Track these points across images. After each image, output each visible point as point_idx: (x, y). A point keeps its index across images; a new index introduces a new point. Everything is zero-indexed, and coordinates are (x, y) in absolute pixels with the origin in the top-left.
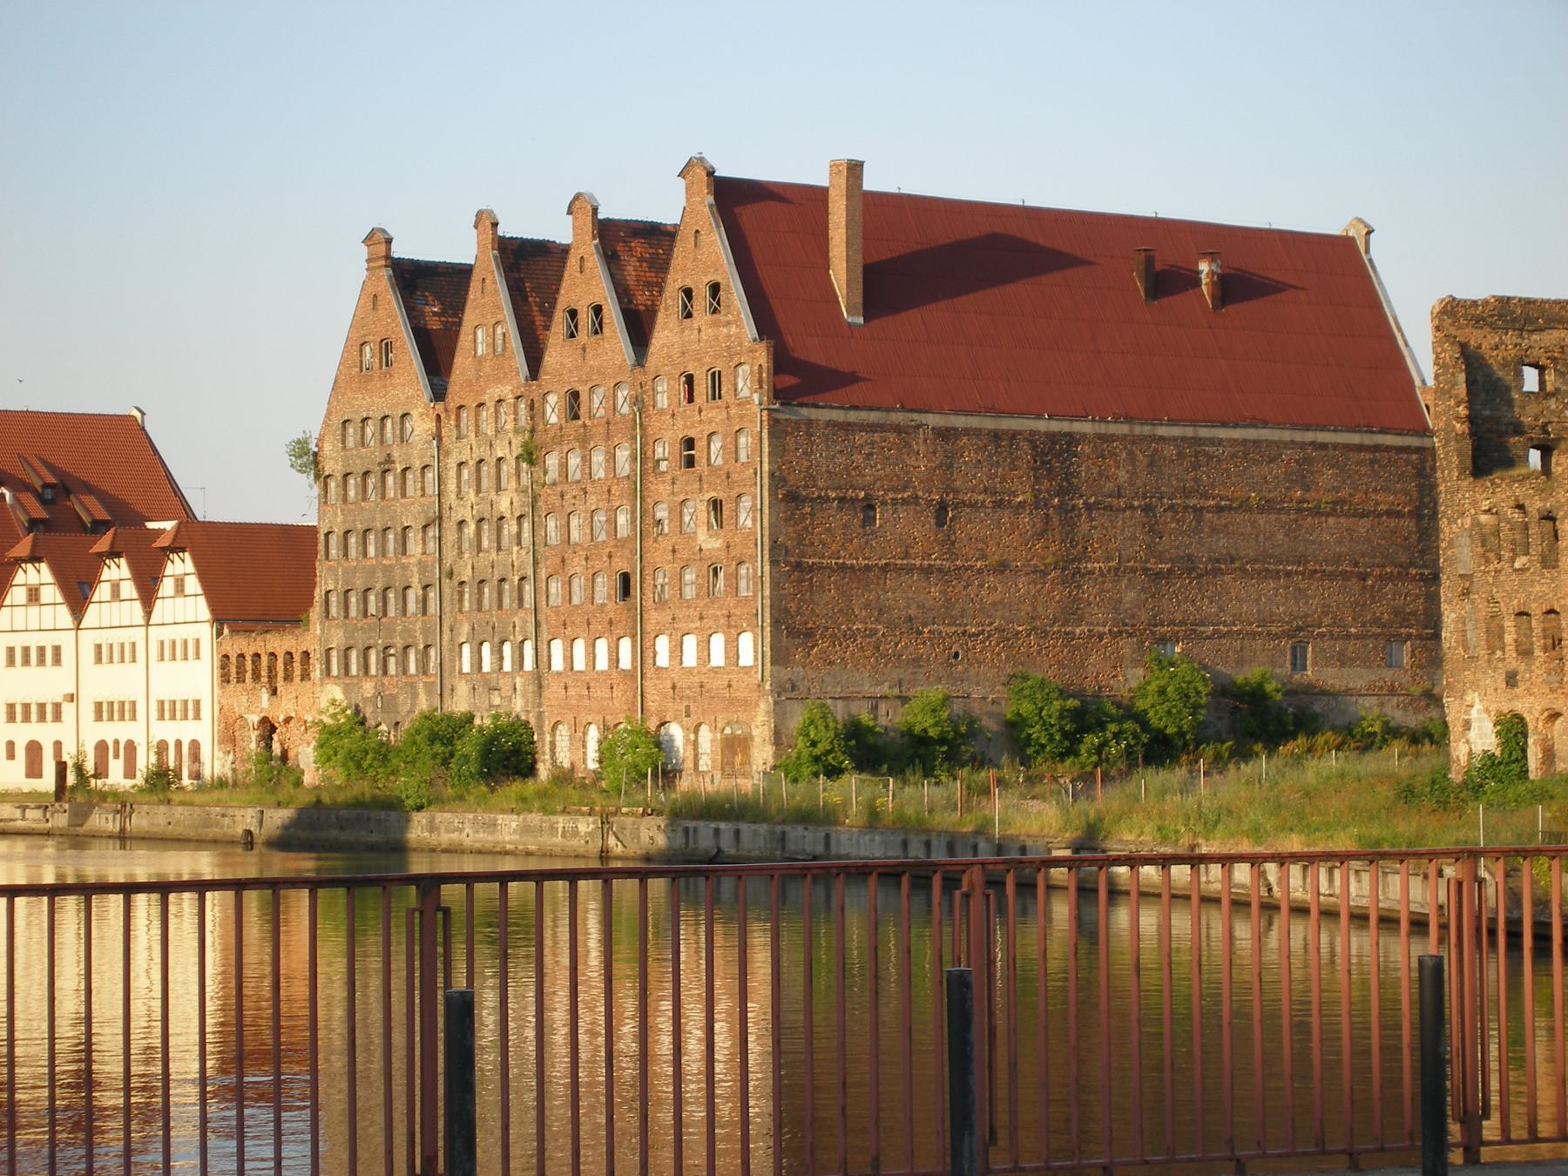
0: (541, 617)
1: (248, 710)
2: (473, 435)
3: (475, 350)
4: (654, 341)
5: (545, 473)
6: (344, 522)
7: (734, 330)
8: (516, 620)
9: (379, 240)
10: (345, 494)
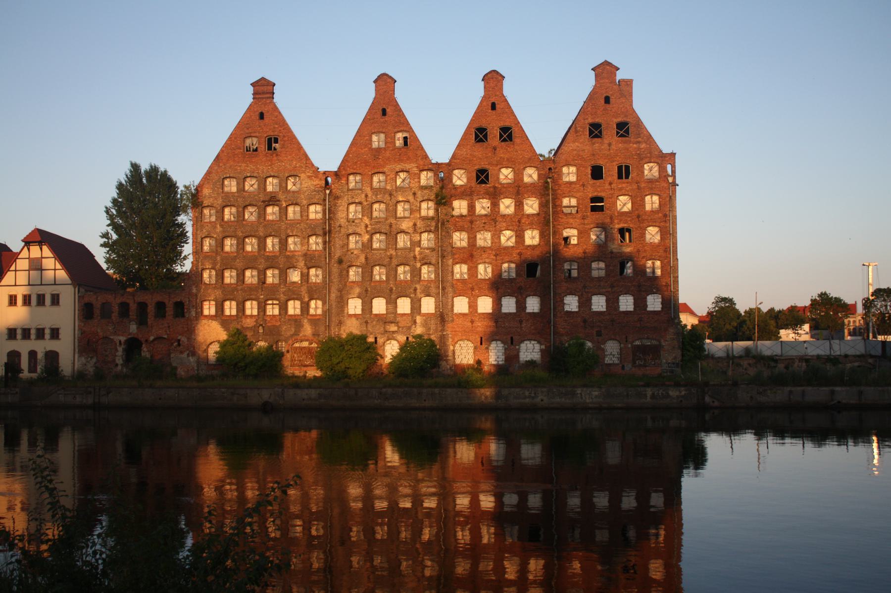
1: (115, 334)
6: (224, 232)
7: (643, 146)
8: (418, 286)
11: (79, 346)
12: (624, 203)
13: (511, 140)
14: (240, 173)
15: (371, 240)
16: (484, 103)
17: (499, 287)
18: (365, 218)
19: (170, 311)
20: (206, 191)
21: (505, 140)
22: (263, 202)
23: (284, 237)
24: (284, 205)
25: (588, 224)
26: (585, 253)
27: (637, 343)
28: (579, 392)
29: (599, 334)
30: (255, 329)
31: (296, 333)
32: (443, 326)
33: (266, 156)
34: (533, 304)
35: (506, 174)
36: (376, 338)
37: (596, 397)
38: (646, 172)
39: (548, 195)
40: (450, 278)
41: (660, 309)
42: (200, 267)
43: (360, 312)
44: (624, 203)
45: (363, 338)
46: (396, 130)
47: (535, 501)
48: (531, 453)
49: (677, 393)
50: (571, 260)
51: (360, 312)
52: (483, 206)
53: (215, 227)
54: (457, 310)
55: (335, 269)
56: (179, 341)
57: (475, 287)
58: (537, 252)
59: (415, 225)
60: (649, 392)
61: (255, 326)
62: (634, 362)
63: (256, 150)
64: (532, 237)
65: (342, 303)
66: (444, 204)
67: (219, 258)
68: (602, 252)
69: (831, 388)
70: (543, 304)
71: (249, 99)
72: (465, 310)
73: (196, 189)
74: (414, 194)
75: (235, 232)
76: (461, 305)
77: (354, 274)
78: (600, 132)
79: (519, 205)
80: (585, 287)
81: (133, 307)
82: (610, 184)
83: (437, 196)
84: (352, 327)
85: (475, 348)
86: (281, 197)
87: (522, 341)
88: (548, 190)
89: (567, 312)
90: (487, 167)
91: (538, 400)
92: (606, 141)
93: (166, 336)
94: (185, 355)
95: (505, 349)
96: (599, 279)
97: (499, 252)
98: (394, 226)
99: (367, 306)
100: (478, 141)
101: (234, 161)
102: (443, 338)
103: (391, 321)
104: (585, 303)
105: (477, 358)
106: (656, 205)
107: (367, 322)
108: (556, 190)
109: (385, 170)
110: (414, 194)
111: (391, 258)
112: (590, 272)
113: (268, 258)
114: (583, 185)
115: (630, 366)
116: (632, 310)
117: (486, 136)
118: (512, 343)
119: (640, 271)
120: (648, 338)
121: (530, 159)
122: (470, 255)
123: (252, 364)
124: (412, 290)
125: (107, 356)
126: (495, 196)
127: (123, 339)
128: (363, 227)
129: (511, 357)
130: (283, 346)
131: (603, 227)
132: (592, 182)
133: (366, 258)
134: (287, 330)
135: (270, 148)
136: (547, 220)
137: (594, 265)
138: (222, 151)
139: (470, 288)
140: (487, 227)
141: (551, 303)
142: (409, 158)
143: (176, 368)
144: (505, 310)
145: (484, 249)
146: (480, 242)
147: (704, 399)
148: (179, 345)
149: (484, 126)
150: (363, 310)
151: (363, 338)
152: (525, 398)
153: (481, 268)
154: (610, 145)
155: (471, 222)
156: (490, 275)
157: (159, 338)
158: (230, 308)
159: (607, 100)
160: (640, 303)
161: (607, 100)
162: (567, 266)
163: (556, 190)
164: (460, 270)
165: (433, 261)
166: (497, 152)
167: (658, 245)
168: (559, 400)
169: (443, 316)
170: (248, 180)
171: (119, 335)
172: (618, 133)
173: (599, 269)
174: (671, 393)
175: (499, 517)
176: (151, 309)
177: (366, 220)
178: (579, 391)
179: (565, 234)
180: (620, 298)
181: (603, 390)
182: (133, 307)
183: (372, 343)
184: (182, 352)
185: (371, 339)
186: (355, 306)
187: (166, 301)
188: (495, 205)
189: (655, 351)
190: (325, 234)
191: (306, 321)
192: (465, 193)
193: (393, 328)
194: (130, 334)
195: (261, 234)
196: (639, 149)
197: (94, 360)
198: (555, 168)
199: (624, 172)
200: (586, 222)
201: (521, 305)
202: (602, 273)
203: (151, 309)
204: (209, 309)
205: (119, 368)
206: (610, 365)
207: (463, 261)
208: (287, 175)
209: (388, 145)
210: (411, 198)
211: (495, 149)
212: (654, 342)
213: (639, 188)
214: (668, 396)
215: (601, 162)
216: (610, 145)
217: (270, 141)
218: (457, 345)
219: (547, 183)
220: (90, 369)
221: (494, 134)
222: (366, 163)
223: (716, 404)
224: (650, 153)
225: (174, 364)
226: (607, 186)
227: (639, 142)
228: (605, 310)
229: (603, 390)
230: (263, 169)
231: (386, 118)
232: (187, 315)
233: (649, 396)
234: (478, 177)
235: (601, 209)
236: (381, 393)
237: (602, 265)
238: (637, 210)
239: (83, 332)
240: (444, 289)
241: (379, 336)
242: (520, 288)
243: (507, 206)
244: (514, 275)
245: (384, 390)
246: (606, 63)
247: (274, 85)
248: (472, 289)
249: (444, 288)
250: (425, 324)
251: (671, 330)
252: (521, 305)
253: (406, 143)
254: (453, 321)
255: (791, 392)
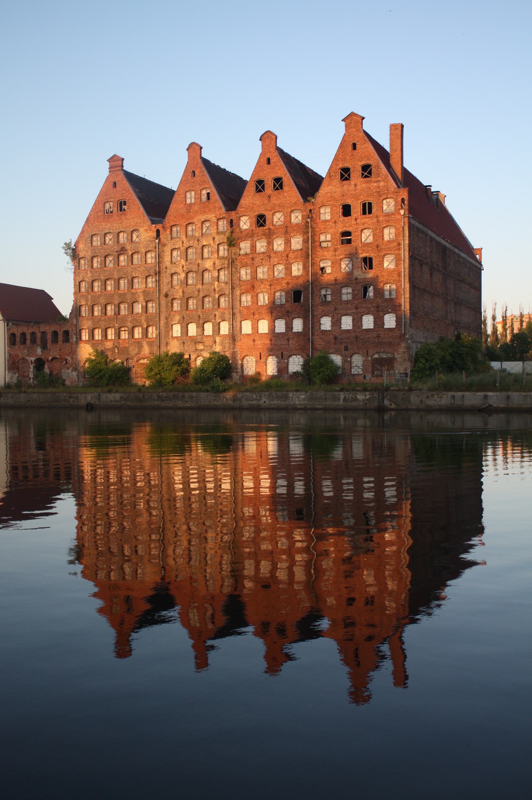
0: (236, 311)
1: (29, 356)
2: (184, 237)
3: (186, 201)
4: (320, 191)
5: (240, 250)
6: (92, 276)
7: (382, 184)
8: (217, 313)
9: (194, 149)
10: (92, 265)
11: (8, 365)
12: (367, 236)
13: (282, 188)
14: (102, 231)
15: (187, 277)
16: (262, 160)
17: (275, 311)
18: (182, 260)
19: (60, 338)
20: (81, 246)
21: (277, 189)
22: (117, 252)
23: (130, 278)
24: (130, 254)
25: (339, 255)
26: (336, 280)
27: (376, 356)
28: (291, 395)
29: (346, 349)
30: (112, 350)
31: (139, 353)
32: (234, 344)
33: (118, 216)
34: (298, 325)
35: (278, 218)
36: (190, 355)
37: (303, 399)
38: (385, 207)
39: (309, 233)
40: (238, 305)
41: (394, 327)
42: (78, 304)
43: (179, 335)
44: (367, 236)
45: (181, 355)
46: (201, 188)
47: (299, 488)
48: (296, 448)
49: (363, 397)
50: (326, 287)
51: (179, 335)
52: (261, 246)
53: (87, 274)
54: (244, 331)
55: (163, 301)
56: (66, 360)
57: (256, 312)
58: (301, 281)
59: (214, 264)
60: (342, 395)
61: (112, 348)
62: (373, 373)
63: (111, 212)
64: (297, 269)
65: (169, 327)
66: (234, 246)
67: (90, 297)
68: (349, 280)
69: (484, 393)
70: (305, 324)
71: (106, 173)
72: (249, 331)
73: (75, 245)
74: (214, 238)
75: (99, 276)
76: (247, 327)
77: (176, 306)
78: (349, 175)
79: (288, 243)
80: (336, 309)
81: (39, 335)
82: (356, 219)
83: (228, 239)
84: (174, 348)
85: (256, 362)
86: (128, 247)
87: (290, 356)
88: (308, 229)
89: (323, 330)
90: (264, 213)
91: (262, 402)
92: (353, 183)
93: (58, 357)
94: (70, 371)
95: (278, 362)
96: (347, 302)
97: (273, 282)
98: (200, 265)
99: (185, 330)
100: (258, 192)
101: (98, 222)
102: (234, 354)
103: (197, 340)
104: (337, 323)
105: (257, 371)
106: (392, 236)
107: (184, 343)
108: (314, 228)
109: (195, 220)
110: (214, 238)
111: (199, 291)
112: (340, 296)
113: (120, 295)
114: (335, 222)
115: (370, 376)
116: (372, 327)
117: (263, 187)
118: (282, 358)
119: (379, 292)
120: (384, 352)
121: (295, 203)
122: (252, 287)
123: (110, 375)
124: (213, 316)
125: (25, 372)
126: (270, 236)
127: (33, 359)
128: (181, 268)
129: (282, 369)
130: (131, 363)
131: (352, 256)
132: (342, 218)
133: (183, 292)
134: (133, 351)
135: (121, 210)
136: (309, 253)
137: (344, 291)
138: (90, 214)
139: (253, 314)
140: (264, 262)
141: (311, 324)
142: (210, 210)
143: (64, 380)
144: (277, 330)
145: (262, 281)
146: (260, 276)
147: (383, 402)
148: (66, 363)
149: (261, 179)
150: (181, 333)
151: (181, 355)
152: (253, 400)
153: (261, 296)
154: (356, 185)
155: (253, 259)
156: (267, 302)
157: (54, 359)
158: (98, 335)
159: (354, 146)
160: (379, 322)
161: (354, 146)
162: (323, 292)
163: (314, 228)
164: (246, 299)
165: (227, 293)
166: (271, 199)
167: (394, 270)
168: (276, 402)
169: (234, 337)
170: (108, 235)
171: (31, 357)
172: (363, 174)
173: (348, 293)
174: (359, 397)
175: (275, 500)
176: (49, 337)
177: (183, 262)
178: (291, 395)
179: (322, 265)
180: (363, 317)
181: (308, 394)
182: (39, 335)
183: (188, 359)
184: (68, 369)
185: (186, 356)
186: (177, 330)
187: (58, 330)
188: (270, 243)
189: (389, 363)
190: (156, 274)
191: (145, 343)
192: (250, 235)
193: (201, 347)
194: (37, 356)
195: (116, 277)
196: (378, 187)
197: (17, 375)
198: (314, 209)
199: (367, 209)
200: (337, 253)
201: (289, 326)
202: (350, 297)
203: (49, 337)
204: (85, 336)
205: (32, 380)
206: (355, 375)
207: (247, 292)
208: (131, 230)
209: (197, 200)
210: (211, 242)
211: (269, 197)
212: (389, 355)
213: (378, 221)
214: (356, 399)
215: (349, 202)
216: (356, 185)
217: (121, 203)
218: (245, 360)
219: (308, 222)
220: (15, 381)
221: (269, 184)
222: (182, 216)
223: (393, 406)
224: (388, 190)
225: (64, 378)
226: (354, 222)
227: (378, 181)
228: (351, 328)
229: (308, 394)
230: (116, 226)
231: (195, 179)
232: (71, 341)
233: (342, 399)
234: (258, 222)
235: (349, 242)
236: (159, 396)
237: (350, 290)
238: (377, 241)
239: (10, 355)
240: (234, 314)
241: (192, 354)
242: (288, 312)
243: (279, 245)
244: (284, 301)
245: (161, 394)
246: (352, 115)
247: (123, 159)
248: (254, 314)
249: (234, 315)
250: (222, 344)
251: (403, 345)
252: (289, 326)
253: (208, 198)
254: (240, 340)
255: (453, 397)
